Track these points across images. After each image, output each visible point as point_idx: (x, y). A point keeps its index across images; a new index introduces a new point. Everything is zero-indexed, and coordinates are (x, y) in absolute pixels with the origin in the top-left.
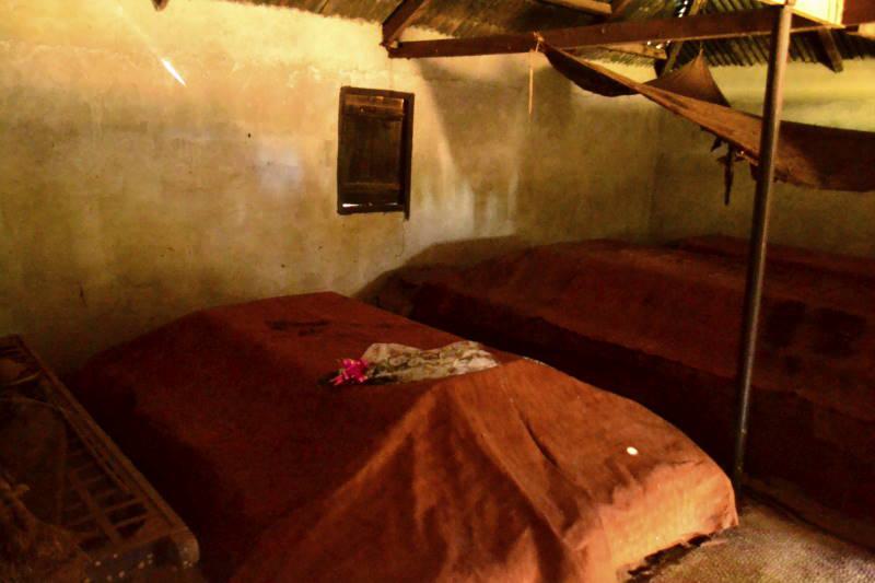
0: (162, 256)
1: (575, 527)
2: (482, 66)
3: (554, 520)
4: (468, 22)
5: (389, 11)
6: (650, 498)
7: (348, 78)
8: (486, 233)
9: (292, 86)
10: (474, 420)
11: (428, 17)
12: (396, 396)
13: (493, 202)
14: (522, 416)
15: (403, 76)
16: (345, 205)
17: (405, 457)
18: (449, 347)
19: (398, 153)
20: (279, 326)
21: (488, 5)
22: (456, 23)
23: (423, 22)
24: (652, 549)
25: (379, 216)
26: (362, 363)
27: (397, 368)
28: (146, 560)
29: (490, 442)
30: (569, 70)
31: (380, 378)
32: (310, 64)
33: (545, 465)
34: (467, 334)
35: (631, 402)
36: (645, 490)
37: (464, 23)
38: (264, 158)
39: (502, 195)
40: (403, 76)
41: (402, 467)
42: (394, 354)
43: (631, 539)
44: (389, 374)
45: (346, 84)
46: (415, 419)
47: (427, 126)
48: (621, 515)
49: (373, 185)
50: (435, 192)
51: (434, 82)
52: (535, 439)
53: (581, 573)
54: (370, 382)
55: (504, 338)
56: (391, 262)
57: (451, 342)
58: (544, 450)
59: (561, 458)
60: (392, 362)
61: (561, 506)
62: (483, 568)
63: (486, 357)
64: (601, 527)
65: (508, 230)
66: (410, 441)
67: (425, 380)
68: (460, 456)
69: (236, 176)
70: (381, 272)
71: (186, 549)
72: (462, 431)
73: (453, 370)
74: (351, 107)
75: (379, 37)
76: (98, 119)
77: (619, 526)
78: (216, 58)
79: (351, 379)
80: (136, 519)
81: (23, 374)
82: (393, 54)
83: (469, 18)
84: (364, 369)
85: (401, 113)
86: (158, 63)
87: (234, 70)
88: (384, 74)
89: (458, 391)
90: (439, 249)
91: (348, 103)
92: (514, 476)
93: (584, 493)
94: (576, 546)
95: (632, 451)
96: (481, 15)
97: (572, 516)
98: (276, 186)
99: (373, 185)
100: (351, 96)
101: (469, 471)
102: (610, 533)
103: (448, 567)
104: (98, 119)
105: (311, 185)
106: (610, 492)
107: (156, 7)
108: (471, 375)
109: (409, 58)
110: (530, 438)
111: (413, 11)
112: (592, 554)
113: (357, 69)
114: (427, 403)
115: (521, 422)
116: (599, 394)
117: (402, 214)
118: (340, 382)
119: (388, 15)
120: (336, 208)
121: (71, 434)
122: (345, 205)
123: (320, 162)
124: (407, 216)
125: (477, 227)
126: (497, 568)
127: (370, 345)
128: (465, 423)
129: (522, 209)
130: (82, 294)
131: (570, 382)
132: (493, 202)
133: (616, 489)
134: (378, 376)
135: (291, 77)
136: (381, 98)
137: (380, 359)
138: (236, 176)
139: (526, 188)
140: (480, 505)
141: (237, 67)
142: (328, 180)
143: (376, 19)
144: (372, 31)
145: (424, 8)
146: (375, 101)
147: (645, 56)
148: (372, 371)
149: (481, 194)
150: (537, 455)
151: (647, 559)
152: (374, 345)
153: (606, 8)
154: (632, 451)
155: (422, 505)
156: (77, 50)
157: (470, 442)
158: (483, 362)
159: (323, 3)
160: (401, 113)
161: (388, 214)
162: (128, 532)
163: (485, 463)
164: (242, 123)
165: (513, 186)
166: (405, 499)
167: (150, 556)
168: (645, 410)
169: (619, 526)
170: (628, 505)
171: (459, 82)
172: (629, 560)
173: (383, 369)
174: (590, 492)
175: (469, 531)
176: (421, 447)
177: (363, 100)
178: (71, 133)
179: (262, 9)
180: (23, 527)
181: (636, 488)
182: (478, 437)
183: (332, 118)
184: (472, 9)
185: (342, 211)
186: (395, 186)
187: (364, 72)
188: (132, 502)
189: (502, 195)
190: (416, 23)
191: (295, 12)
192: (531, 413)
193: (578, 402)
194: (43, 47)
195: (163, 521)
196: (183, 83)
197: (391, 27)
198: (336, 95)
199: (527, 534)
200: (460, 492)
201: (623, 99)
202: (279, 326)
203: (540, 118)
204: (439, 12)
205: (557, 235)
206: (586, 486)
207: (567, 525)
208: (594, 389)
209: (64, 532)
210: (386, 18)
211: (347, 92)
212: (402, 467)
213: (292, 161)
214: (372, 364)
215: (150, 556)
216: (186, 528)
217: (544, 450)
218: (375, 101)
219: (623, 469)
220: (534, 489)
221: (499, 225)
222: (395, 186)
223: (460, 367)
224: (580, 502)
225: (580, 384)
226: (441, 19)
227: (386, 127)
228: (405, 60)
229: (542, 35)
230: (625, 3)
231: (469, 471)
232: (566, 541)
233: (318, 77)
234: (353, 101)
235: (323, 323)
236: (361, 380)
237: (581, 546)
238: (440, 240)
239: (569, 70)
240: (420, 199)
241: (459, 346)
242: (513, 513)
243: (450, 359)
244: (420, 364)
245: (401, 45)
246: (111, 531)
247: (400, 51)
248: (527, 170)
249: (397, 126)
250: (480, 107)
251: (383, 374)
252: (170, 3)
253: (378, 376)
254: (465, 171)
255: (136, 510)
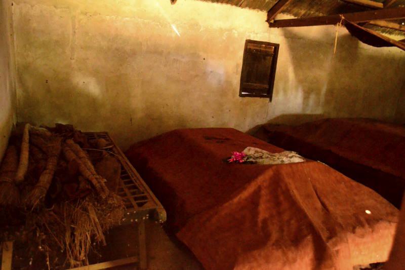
0: (163, 108)
1: (334, 239)
2: (313, 32)
3: (324, 235)
4: (308, 12)
5: (271, 6)
6: (375, 236)
7: (250, 36)
8: (308, 112)
9: (224, 38)
10: (290, 184)
11: (289, 8)
12: (256, 169)
13: (313, 97)
14: (314, 186)
15: (275, 36)
16: (243, 93)
17: (257, 193)
18: (283, 153)
19: (269, 71)
20: (208, 138)
21: (319, 3)
22: (303, 12)
23: (287, 11)
24: (374, 261)
25: (258, 99)
26: (242, 155)
27: (257, 158)
28: (146, 217)
29: (295, 193)
30: (359, 34)
31: (249, 161)
32: (233, 29)
33: (323, 211)
34: (290, 149)
35: (371, 190)
36: (373, 231)
37: (306, 12)
38: (209, 69)
39: (318, 94)
40: (275, 36)
41: (254, 201)
42: (256, 152)
43: (363, 253)
44: (254, 160)
45: (248, 39)
46: (263, 179)
47: (284, 60)
48: (358, 240)
49: (257, 85)
50: (285, 91)
51: (289, 39)
52: (319, 198)
53: (334, 260)
54: (245, 163)
55: (309, 153)
56: (261, 121)
57: (283, 151)
58: (323, 204)
59: (331, 209)
60: (256, 155)
61: (328, 229)
62: (286, 248)
63: (299, 157)
64: (347, 243)
65: (319, 111)
66: (259, 188)
67: (269, 164)
68: (282, 198)
69: (197, 76)
70: (257, 124)
71: (161, 215)
72: (284, 188)
73: (283, 161)
74: (250, 49)
75: (265, 18)
76: (144, 48)
77: (357, 245)
78: (194, 25)
79: (236, 161)
80: (143, 201)
81: (107, 145)
82: (271, 25)
83: (309, 10)
84: (243, 157)
85: (273, 53)
86: (170, 26)
87: (201, 30)
88: (266, 34)
89: (284, 172)
90: (284, 117)
91: (248, 47)
92: (306, 211)
93: (340, 226)
94: (334, 247)
95: (368, 212)
96: (315, 7)
97: (332, 234)
98: (213, 82)
99: (257, 85)
100: (250, 44)
101: (285, 205)
102: (352, 246)
103: (270, 243)
104: (144, 48)
105: (229, 82)
106: (354, 228)
107: (172, 3)
108: (291, 165)
109: (278, 28)
110: (316, 197)
111: (282, 6)
112: (341, 254)
113: (254, 32)
114: (269, 173)
115: (313, 190)
116: (354, 183)
117: (268, 99)
118: (232, 161)
119: (270, 8)
120: (238, 94)
121: (123, 168)
122: (243, 93)
123: (234, 73)
124: (271, 100)
125: (304, 109)
126: (293, 248)
127: (246, 147)
128: (286, 185)
129: (327, 102)
130: (131, 120)
131: (339, 175)
132: (313, 97)
133: (358, 227)
134: (249, 160)
135: (224, 34)
136: (264, 46)
137: (250, 153)
138: (197, 76)
139: (330, 92)
140: (289, 221)
141: (202, 29)
142: (236, 80)
143: (265, 9)
144: (263, 15)
145: (287, 5)
146: (260, 47)
147: (401, 31)
148: (246, 158)
149: (307, 94)
150: (319, 205)
151: (371, 265)
152: (248, 148)
153: (380, 5)
154: (368, 212)
155: (261, 217)
156: (139, 20)
157: (287, 193)
158: (297, 159)
159: (242, 2)
160: (273, 53)
161: (262, 99)
162: (140, 205)
163: (293, 203)
164: (201, 53)
165: (324, 90)
166: (255, 214)
167: (148, 215)
168: (377, 194)
169: (357, 245)
170: (363, 236)
171: (302, 40)
172: (361, 263)
173: (251, 157)
174: (344, 226)
175: (281, 230)
176: (263, 192)
177: (256, 46)
178: (134, 54)
179: (215, 5)
180: (104, 191)
181: (368, 229)
182: (291, 191)
183: (241, 53)
184: (311, 6)
185: (241, 95)
186: (267, 86)
187: (257, 34)
188: (142, 195)
189: (318, 94)
190: (283, 12)
191: (229, 6)
192: (318, 186)
193: (343, 185)
194: (127, 19)
195: (154, 203)
196: (179, 35)
197: (271, 13)
198: (244, 43)
199: (309, 237)
200: (280, 214)
201: (386, 50)
202: (208, 138)
203: (341, 60)
204: (294, 7)
205: (344, 115)
206: (342, 223)
207: (330, 238)
208: (352, 181)
209: (118, 197)
210: (269, 9)
211: (249, 42)
212: (254, 201)
213: (221, 71)
214: (246, 155)
215: (148, 215)
216: (162, 207)
217: (323, 204)
218: (260, 47)
219: (362, 219)
220: (316, 219)
221: (315, 108)
222: (267, 86)
223: (286, 160)
224: (338, 229)
225: (344, 176)
226: (295, 10)
227: (265, 59)
228: (276, 28)
229: (344, 16)
230: (392, 2)
231: (285, 205)
232: (329, 244)
233: (236, 35)
234: (250, 46)
235: (228, 139)
236: (241, 161)
237: (336, 249)
238: (285, 113)
239: (359, 34)
240: (277, 93)
241: (287, 152)
242: (304, 227)
243: (283, 157)
244: (268, 157)
245: (275, 21)
246: (134, 203)
247: (274, 24)
248: (331, 83)
249: (270, 59)
250: (311, 52)
251: (251, 160)
252: (177, 2)
253: (249, 160)
254: (300, 81)
255: (144, 198)
